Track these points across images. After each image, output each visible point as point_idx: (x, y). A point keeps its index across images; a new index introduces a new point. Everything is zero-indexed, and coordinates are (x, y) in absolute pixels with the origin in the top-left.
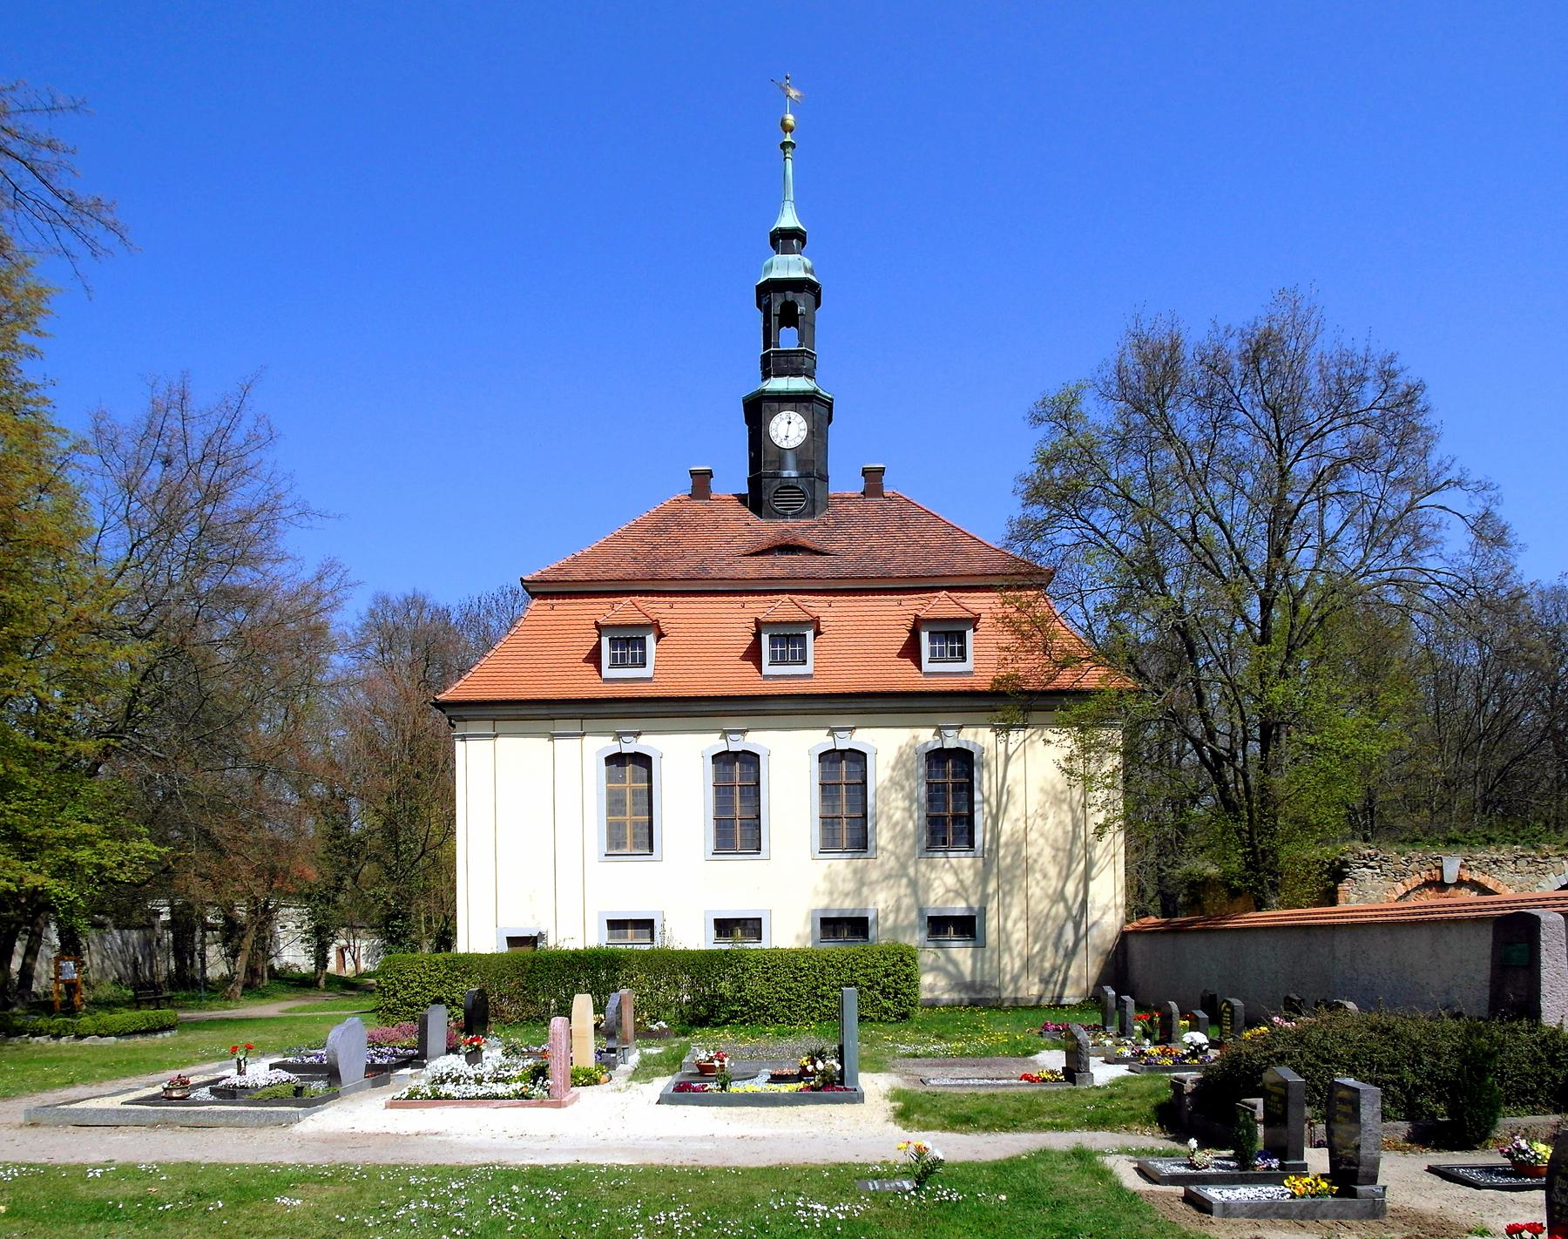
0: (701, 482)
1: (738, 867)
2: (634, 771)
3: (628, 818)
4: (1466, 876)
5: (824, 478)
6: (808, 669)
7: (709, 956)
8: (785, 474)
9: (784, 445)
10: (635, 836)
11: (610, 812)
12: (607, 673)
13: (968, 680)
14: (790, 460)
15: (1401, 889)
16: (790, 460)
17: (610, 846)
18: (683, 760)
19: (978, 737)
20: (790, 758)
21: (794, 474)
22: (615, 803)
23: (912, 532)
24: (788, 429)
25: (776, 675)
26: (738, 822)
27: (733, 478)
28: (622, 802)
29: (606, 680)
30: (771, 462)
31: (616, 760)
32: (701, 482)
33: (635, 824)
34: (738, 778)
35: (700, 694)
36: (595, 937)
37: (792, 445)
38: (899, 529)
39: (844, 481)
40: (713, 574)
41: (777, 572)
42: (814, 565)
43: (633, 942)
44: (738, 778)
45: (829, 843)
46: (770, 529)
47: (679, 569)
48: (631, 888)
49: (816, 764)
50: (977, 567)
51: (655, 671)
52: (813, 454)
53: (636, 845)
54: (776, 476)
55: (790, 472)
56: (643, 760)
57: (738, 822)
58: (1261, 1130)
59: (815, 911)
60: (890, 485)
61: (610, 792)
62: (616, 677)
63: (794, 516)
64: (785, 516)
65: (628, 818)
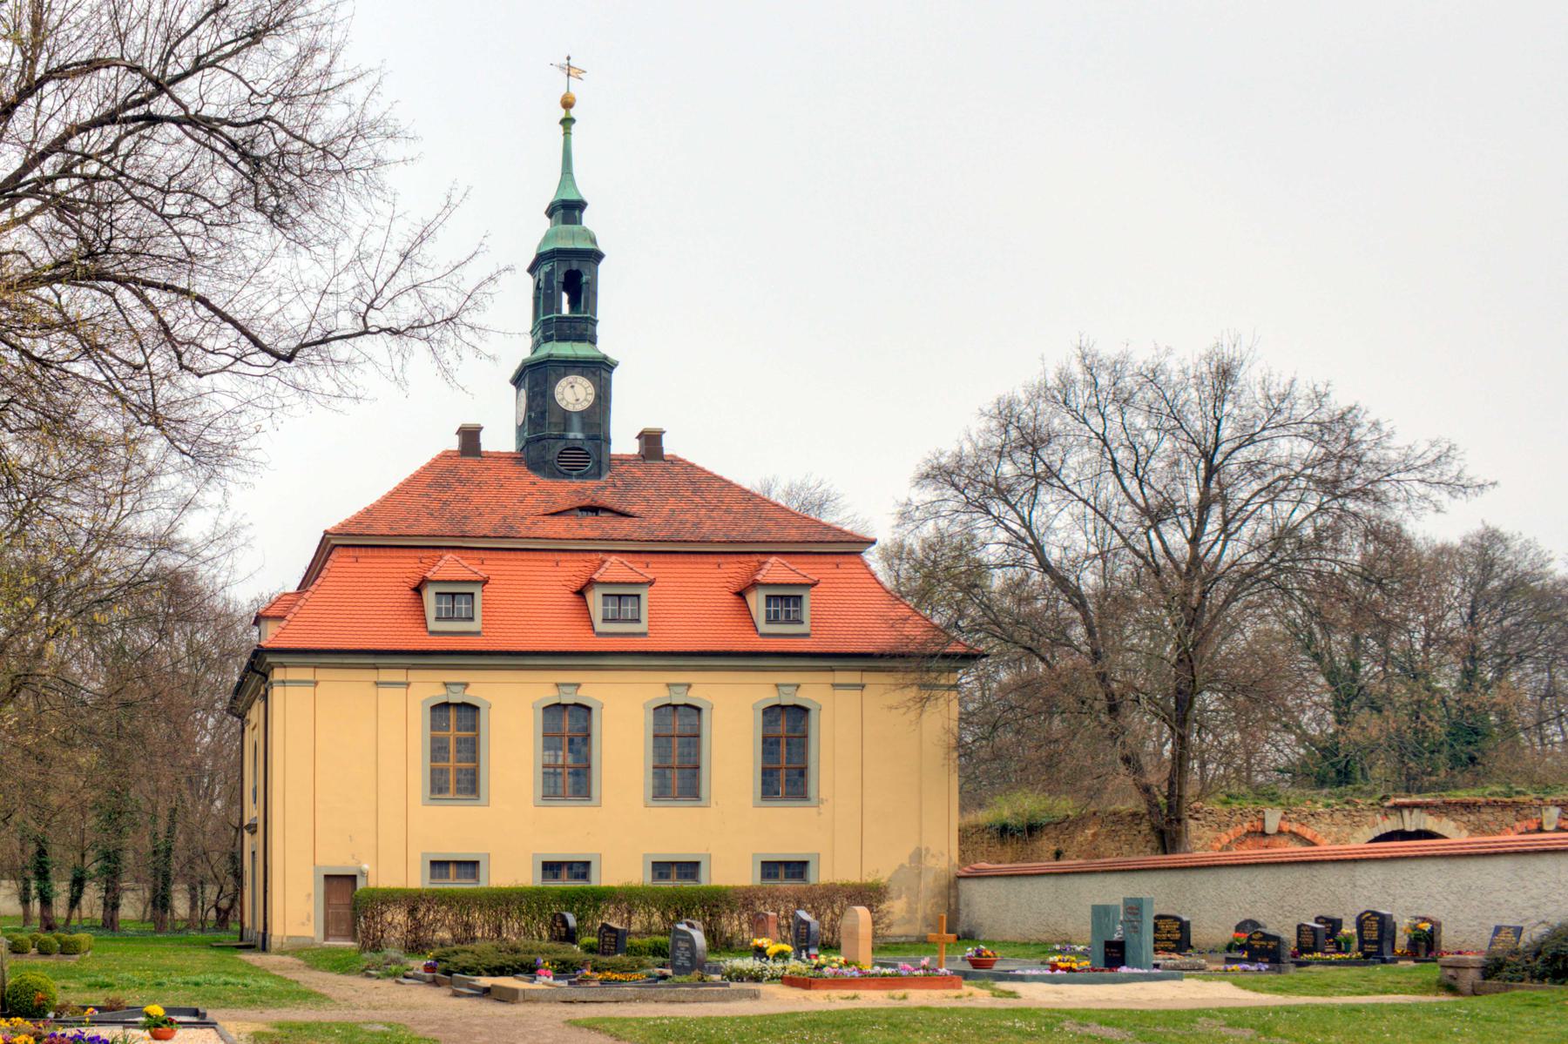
0: (470, 437)
1: (568, 813)
2: (459, 719)
3: (452, 764)
4: (1286, 827)
5: (608, 441)
6: (475, 626)
7: (539, 892)
8: (571, 435)
9: (570, 408)
10: (458, 781)
11: (433, 759)
12: (433, 625)
13: (808, 641)
14: (576, 422)
15: (1225, 839)
16: (576, 422)
17: (432, 791)
18: (512, 709)
19: (811, 689)
20: (623, 710)
21: (580, 436)
22: (438, 750)
23: (710, 497)
24: (573, 393)
25: (604, 630)
26: (678, 768)
27: (501, 437)
28: (445, 749)
29: (432, 633)
30: (556, 425)
31: (441, 708)
32: (470, 437)
33: (459, 770)
34: (569, 730)
35: (676, 649)
36: (418, 879)
37: (579, 408)
38: (694, 492)
39: (623, 442)
40: (524, 533)
41: (581, 533)
42: (623, 527)
43: (565, 884)
44: (569, 730)
45: (437, 787)
46: (566, 491)
47: (483, 525)
48: (454, 829)
49: (540, 713)
50: (794, 534)
51: (477, 629)
52: (597, 416)
53: (459, 791)
54: (561, 437)
55: (576, 434)
56: (471, 709)
57: (678, 768)
58: (71, 1032)
59: (645, 855)
60: (669, 447)
61: (433, 740)
62: (438, 629)
63: (580, 476)
64: (570, 476)
65: (452, 764)
